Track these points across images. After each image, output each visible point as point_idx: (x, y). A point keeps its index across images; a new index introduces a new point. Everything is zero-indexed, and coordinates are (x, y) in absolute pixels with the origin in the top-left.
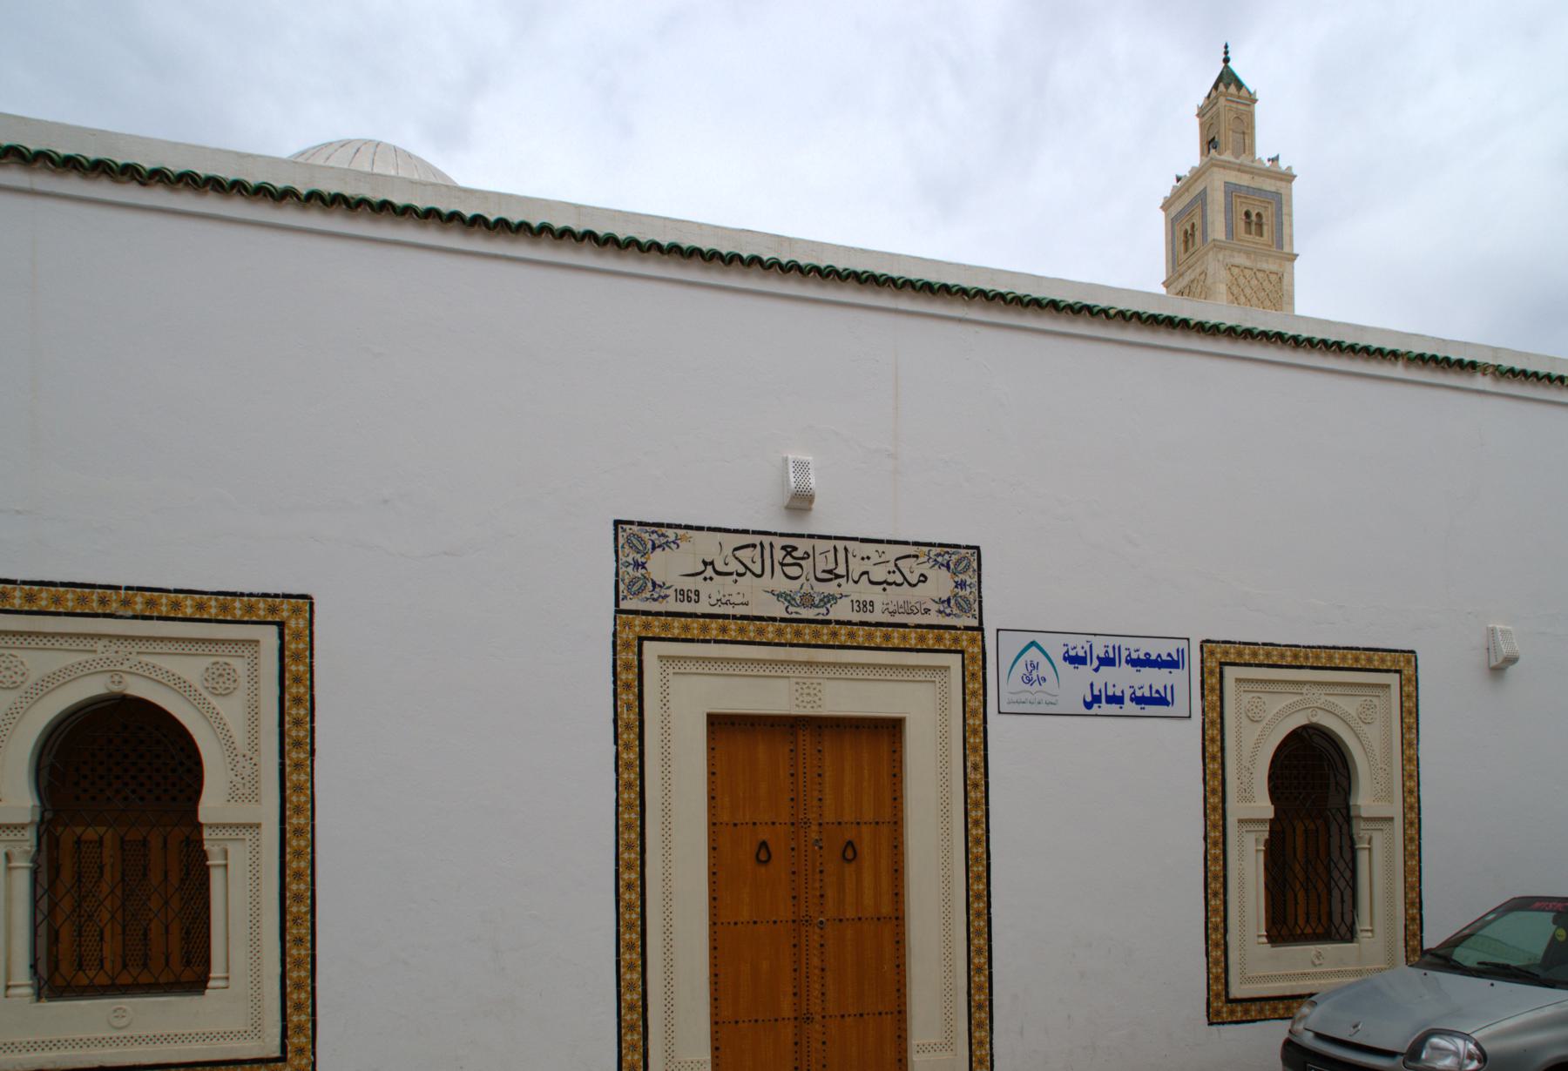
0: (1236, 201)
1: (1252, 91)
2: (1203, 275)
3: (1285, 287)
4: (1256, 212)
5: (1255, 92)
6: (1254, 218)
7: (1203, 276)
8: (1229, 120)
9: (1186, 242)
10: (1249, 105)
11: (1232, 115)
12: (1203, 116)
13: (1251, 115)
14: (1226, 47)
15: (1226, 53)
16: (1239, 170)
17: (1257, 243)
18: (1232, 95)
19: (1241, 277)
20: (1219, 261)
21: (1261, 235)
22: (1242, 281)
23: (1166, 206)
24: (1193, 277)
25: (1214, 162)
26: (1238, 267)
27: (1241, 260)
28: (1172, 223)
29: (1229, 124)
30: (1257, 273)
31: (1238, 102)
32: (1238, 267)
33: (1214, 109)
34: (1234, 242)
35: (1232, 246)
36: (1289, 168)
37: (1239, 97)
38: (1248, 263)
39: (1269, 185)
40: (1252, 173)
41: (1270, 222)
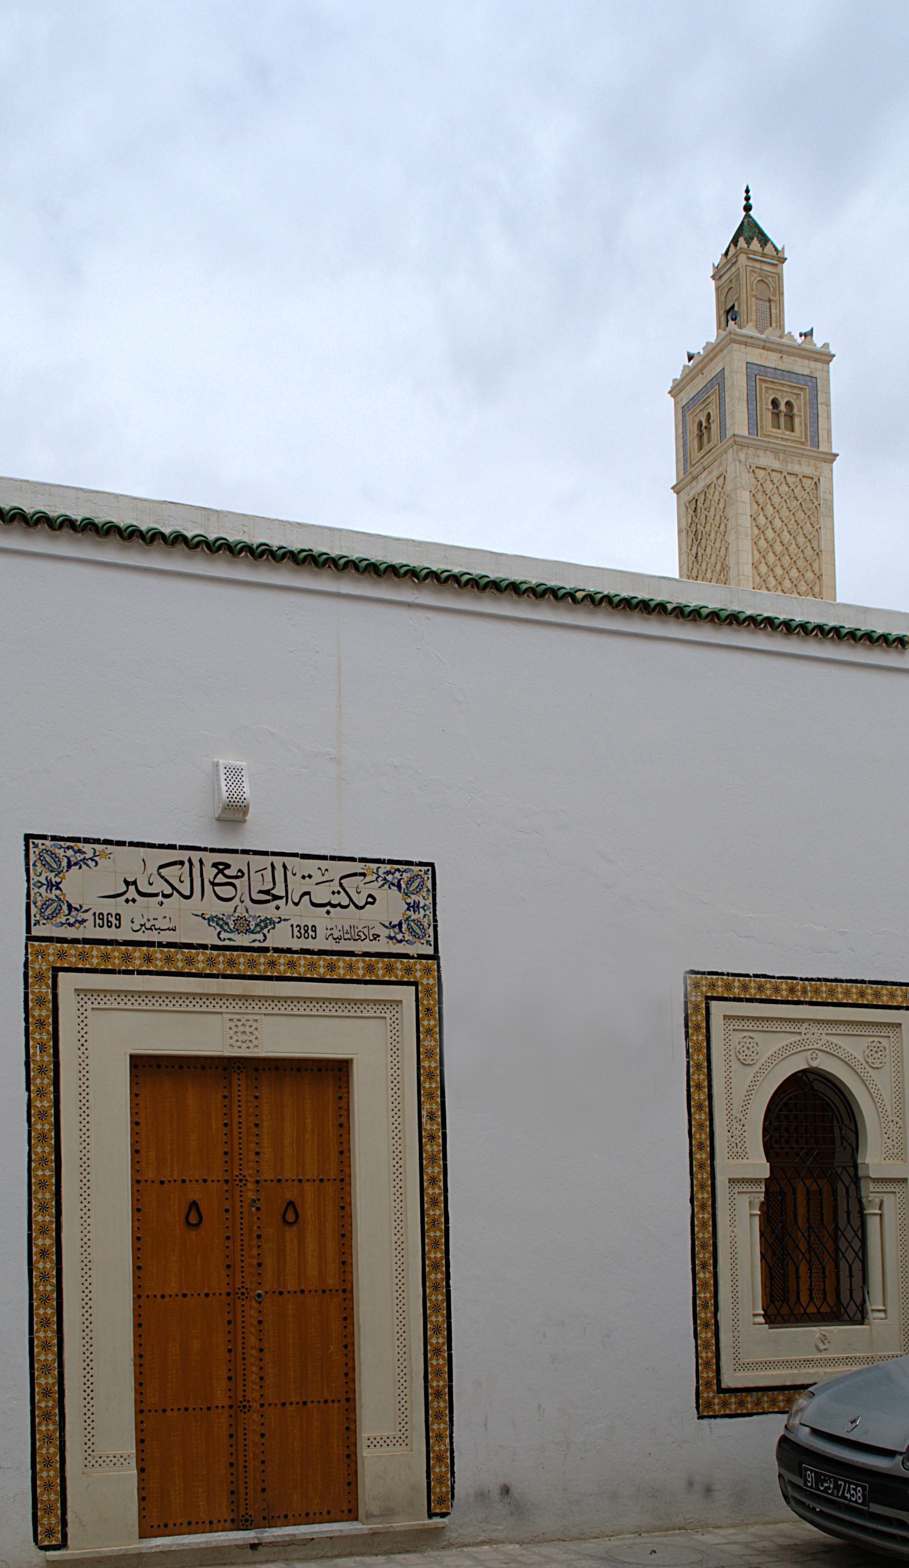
0: (761, 388)
1: (780, 248)
2: (722, 479)
3: (822, 495)
4: (786, 400)
5: (783, 249)
6: (783, 407)
8: (752, 285)
9: (700, 437)
10: (776, 265)
11: (755, 278)
12: (721, 277)
13: (780, 277)
14: (747, 191)
15: (747, 199)
16: (764, 348)
17: (786, 440)
18: (754, 253)
19: (768, 482)
20: (740, 461)
21: (793, 430)
22: (769, 486)
23: (675, 392)
24: (708, 481)
25: (733, 337)
26: (764, 469)
27: (767, 460)
28: (684, 412)
29: (752, 290)
30: (788, 477)
31: (762, 262)
32: (764, 469)
33: (733, 269)
34: (759, 438)
35: (757, 443)
36: (826, 345)
37: (764, 255)
38: (776, 465)
39: (801, 367)
40: (781, 352)
41: (802, 414)
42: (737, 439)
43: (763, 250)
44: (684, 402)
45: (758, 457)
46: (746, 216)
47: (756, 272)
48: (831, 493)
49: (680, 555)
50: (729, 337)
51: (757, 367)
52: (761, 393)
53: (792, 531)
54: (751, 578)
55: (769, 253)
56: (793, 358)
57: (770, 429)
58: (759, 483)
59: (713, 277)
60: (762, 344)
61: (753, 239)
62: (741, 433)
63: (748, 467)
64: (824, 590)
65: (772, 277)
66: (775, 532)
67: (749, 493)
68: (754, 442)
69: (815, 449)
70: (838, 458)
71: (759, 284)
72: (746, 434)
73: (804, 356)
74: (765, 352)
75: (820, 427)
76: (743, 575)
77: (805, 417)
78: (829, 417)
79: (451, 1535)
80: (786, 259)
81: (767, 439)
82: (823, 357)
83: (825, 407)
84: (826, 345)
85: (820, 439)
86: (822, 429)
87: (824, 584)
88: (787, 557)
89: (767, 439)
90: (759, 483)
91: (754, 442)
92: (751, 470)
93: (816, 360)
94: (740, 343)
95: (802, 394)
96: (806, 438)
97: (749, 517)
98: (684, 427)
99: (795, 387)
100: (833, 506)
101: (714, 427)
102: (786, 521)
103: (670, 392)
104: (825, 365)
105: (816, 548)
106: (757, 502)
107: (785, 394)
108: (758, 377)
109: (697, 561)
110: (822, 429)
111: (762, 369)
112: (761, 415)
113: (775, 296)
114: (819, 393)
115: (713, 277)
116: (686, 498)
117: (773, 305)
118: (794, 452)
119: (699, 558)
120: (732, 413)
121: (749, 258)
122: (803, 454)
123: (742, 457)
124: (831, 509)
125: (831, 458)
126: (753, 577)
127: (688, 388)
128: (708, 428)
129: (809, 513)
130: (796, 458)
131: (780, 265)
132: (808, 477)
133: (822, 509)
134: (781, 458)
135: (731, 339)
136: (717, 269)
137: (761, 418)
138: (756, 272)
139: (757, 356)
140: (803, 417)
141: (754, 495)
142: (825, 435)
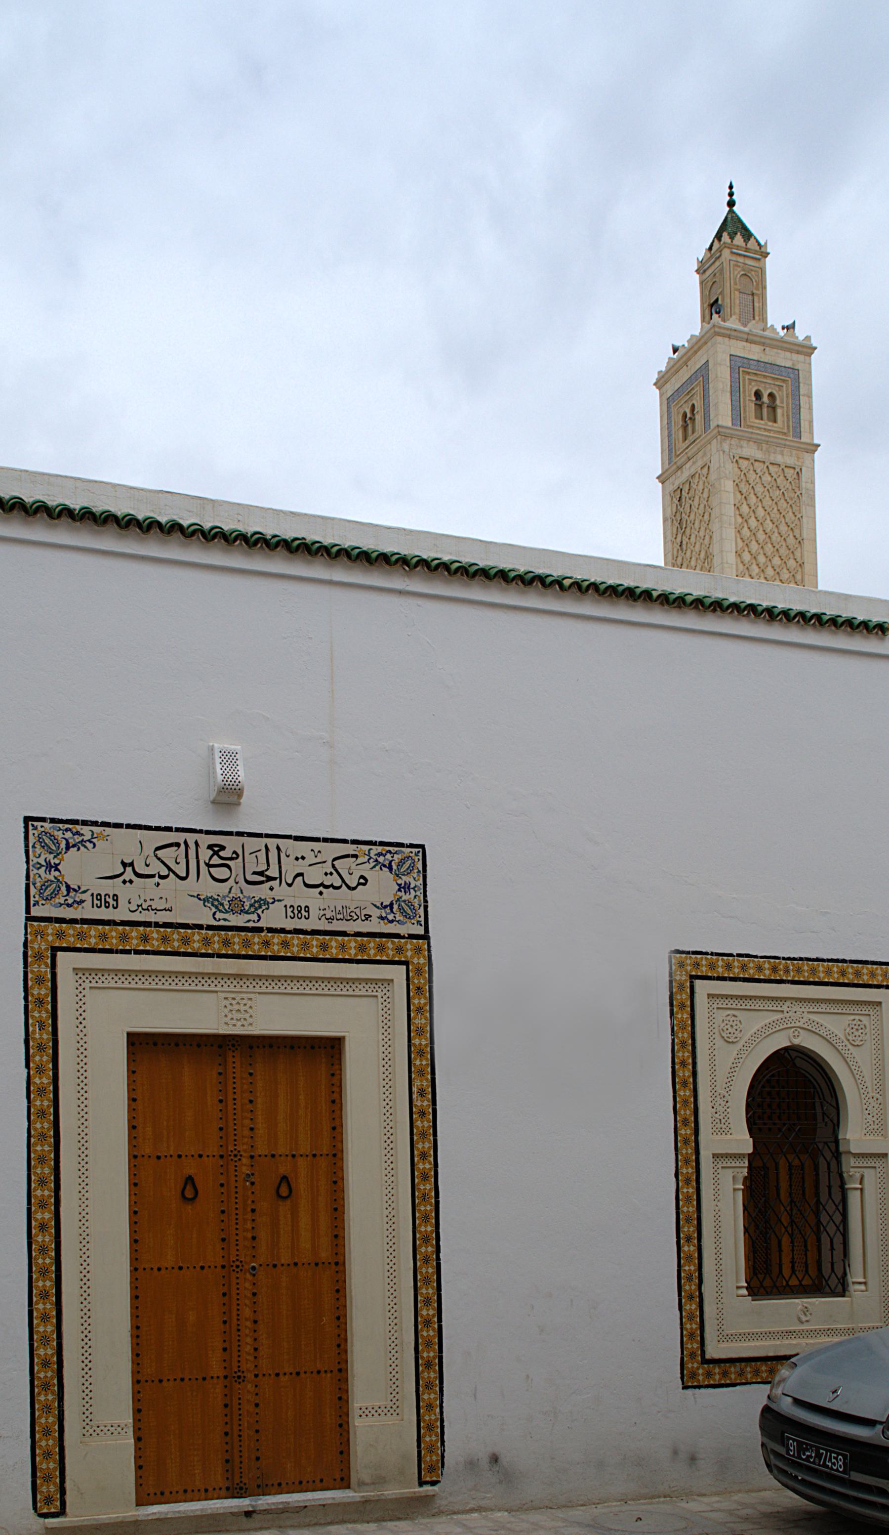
0: (744, 380)
1: (762, 243)
2: (706, 469)
3: (803, 485)
4: (769, 391)
5: (766, 243)
6: (765, 399)
7: (706, 469)
8: (735, 279)
9: (685, 428)
10: (759, 260)
11: (739, 272)
12: (705, 271)
13: (763, 271)
14: (731, 187)
15: (731, 195)
16: (747, 341)
17: (769, 431)
18: (738, 247)
19: (751, 472)
20: (724, 452)
21: (775, 421)
22: (752, 476)
23: (660, 383)
24: (693, 471)
25: (717, 329)
26: (748, 459)
27: (750, 450)
28: (669, 403)
29: (736, 284)
30: (771, 467)
31: (745, 256)
32: (748, 459)
33: (717, 264)
34: (742, 429)
35: (740, 433)
36: (808, 338)
37: (747, 250)
38: (759, 455)
39: (784, 359)
40: (763, 344)
41: (785, 405)
42: (720, 430)
43: (746, 245)
44: (669, 394)
45: (742, 447)
46: (729, 211)
47: (739, 266)
48: (813, 483)
49: (665, 543)
50: (713, 330)
51: (741, 359)
52: (744, 385)
53: (775, 520)
54: (734, 566)
55: (752, 248)
56: (775, 350)
57: (753, 420)
58: (743, 473)
59: (697, 271)
60: (745, 336)
61: (736, 234)
62: (724, 424)
63: (732, 457)
64: (806, 577)
65: (755, 271)
66: (758, 521)
67: (732, 483)
68: (737, 433)
69: (797, 440)
70: (819, 448)
71: (742, 278)
72: (730, 425)
73: (786, 348)
74: (749, 345)
75: (802, 418)
76: (727, 563)
77: (788, 408)
78: (810, 408)
79: (441, 1503)
80: (768, 254)
81: (750, 430)
82: (805, 350)
83: (807, 399)
84: (808, 338)
85: (802, 430)
86: (804, 420)
87: (806, 571)
88: (770, 545)
89: (750, 430)
90: (743, 473)
91: (737, 433)
92: (735, 460)
93: (798, 352)
94: (724, 335)
95: (785, 385)
96: (788, 429)
97: (733, 506)
98: (669, 418)
99: (777, 378)
100: (814, 495)
101: (698, 418)
102: (769, 510)
103: (655, 384)
104: (807, 358)
105: (798, 536)
106: (740, 492)
107: (768, 386)
108: (741, 369)
109: (682, 550)
110: (804, 420)
111: (745, 361)
112: (745, 406)
113: (758, 290)
114: (801, 385)
115: (697, 271)
116: (671, 488)
117: (756, 298)
118: (776, 443)
119: (684, 547)
120: (716, 405)
121: (732, 253)
122: (785, 445)
123: (726, 447)
124: (812, 498)
125: (813, 448)
126: (737, 565)
127: (673, 380)
128: (693, 419)
129: (791, 502)
130: (778, 449)
131: (763, 259)
132: (790, 467)
133: (804, 498)
134: (764, 449)
135: (715, 332)
136: (701, 263)
137: (744, 409)
138: (739, 266)
139: (740, 349)
140: (785, 408)
141: (737, 484)
142: (807, 426)
